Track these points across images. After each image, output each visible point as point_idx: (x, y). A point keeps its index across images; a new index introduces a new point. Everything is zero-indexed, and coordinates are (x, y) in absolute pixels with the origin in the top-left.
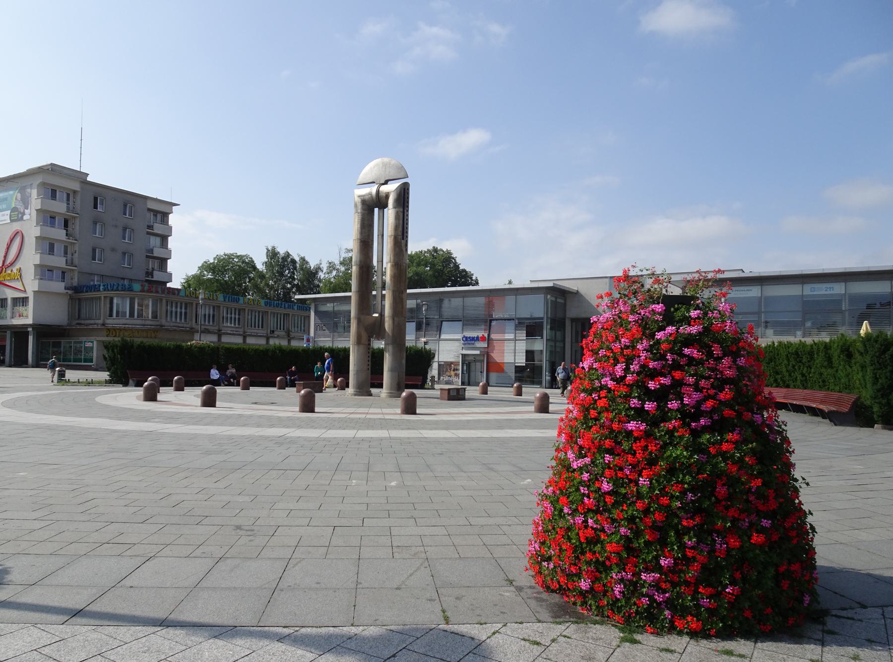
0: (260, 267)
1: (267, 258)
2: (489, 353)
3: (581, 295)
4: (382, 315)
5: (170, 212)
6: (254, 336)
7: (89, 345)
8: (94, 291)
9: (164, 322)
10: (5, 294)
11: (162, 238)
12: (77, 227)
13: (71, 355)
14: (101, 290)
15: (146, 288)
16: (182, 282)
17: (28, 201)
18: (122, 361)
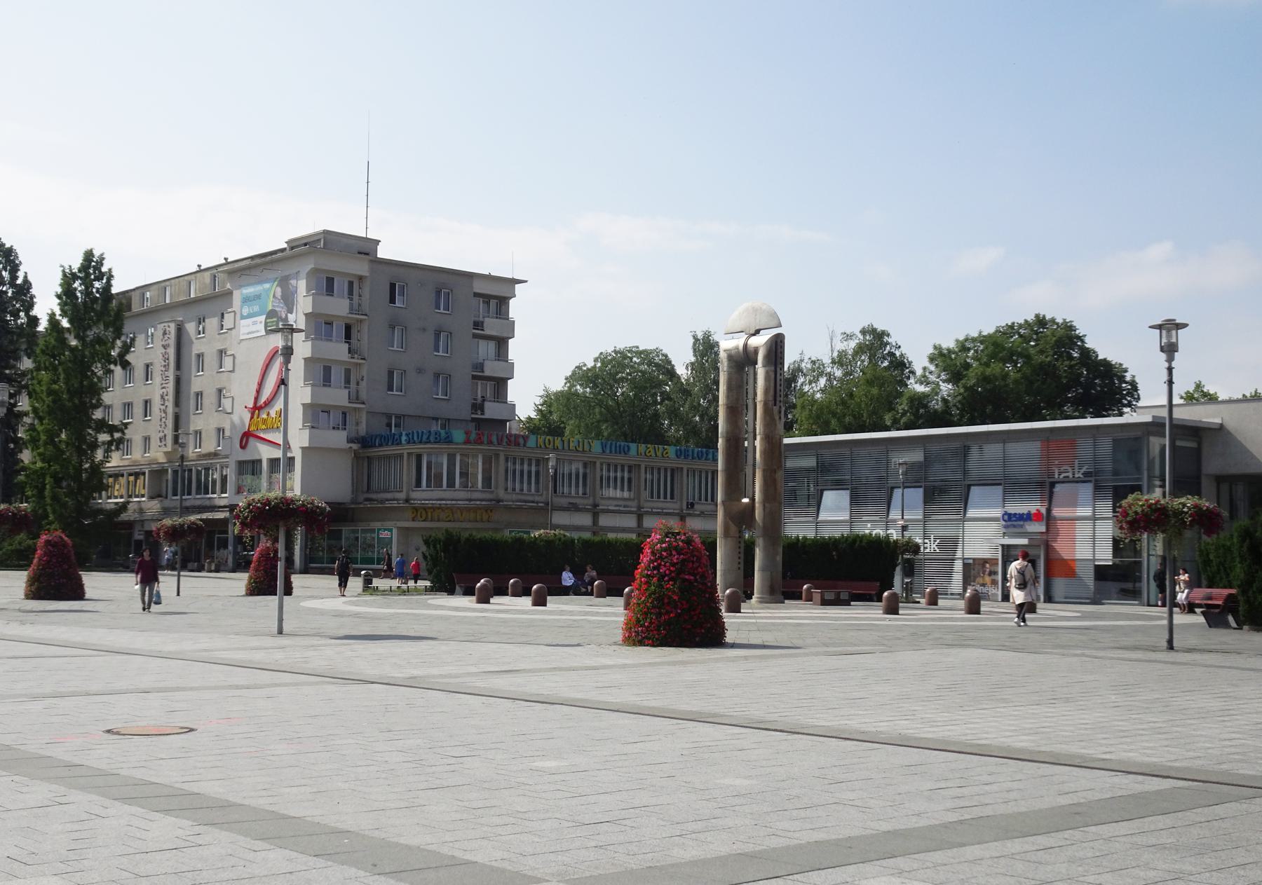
0: (682, 371)
1: (695, 355)
2: (1050, 543)
3: (1229, 433)
4: (753, 499)
5: (511, 336)
6: (658, 513)
7: (385, 535)
8: (392, 444)
9: (501, 494)
10: (260, 455)
11: (499, 342)
12: (366, 337)
13: (358, 552)
14: (403, 442)
15: (473, 436)
16: (538, 403)
17: (293, 300)
18: (446, 561)
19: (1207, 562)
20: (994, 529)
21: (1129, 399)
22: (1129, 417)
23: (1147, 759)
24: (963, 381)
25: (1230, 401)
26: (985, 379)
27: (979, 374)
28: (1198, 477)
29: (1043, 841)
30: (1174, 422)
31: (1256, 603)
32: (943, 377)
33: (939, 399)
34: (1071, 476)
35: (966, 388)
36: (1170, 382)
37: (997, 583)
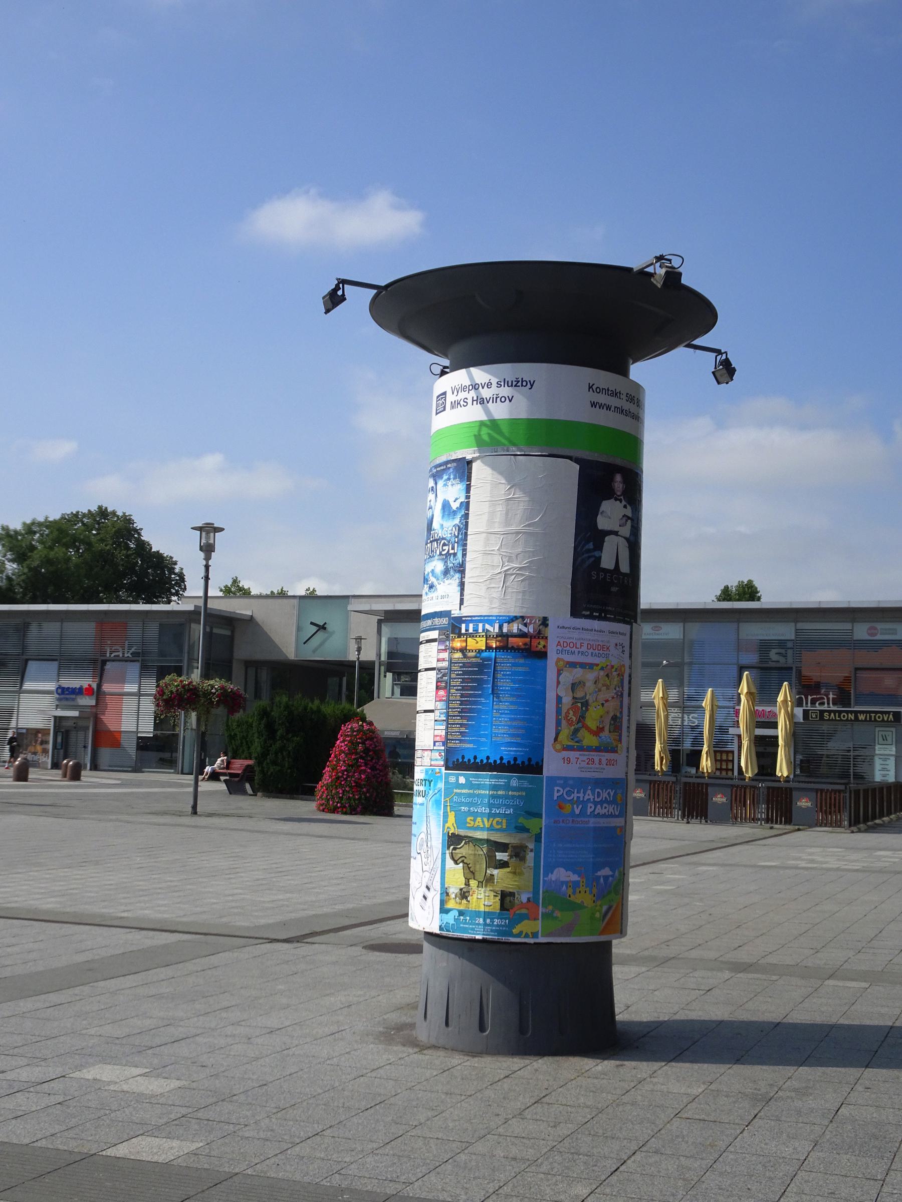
19: (232, 737)
20: (47, 702)
21: (177, 588)
22: (176, 605)
23: (159, 916)
24: (28, 562)
25: (260, 597)
26: (48, 562)
27: (43, 556)
28: (229, 662)
29: (53, 998)
30: (208, 611)
31: (269, 773)
32: (9, 556)
33: (4, 577)
34: (121, 655)
35: (30, 569)
36: (207, 578)
37: (48, 752)
